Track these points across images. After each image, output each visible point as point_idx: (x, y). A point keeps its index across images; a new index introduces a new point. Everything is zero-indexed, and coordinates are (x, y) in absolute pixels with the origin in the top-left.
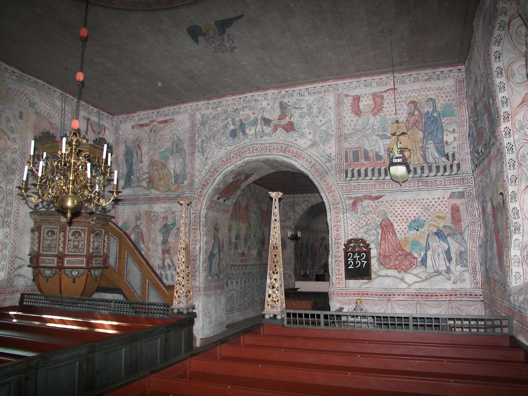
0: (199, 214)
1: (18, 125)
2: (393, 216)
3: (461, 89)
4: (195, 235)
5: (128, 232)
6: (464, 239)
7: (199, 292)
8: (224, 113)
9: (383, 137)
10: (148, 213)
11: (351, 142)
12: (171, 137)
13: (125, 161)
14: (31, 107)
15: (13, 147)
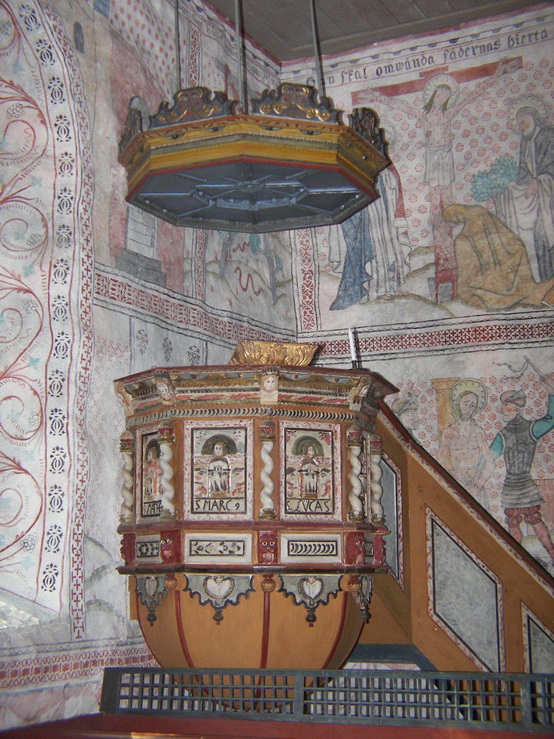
12: (515, 123)
15: (58, 153)
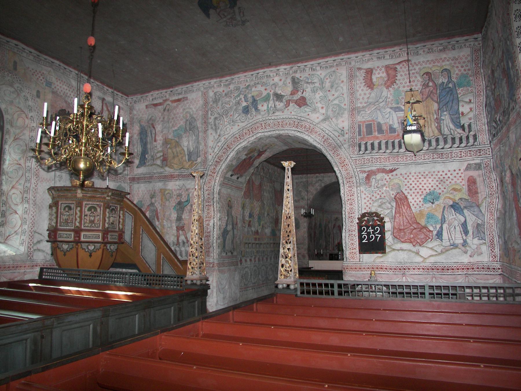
0: (212, 191)
1: (35, 104)
2: (407, 188)
3: (478, 58)
4: (209, 211)
5: (143, 210)
6: (481, 211)
7: (214, 268)
8: (237, 90)
9: (397, 109)
10: (163, 191)
11: (365, 115)
12: (184, 116)
13: (139, 140)
14: (48, 86)
15: (31, 126)
